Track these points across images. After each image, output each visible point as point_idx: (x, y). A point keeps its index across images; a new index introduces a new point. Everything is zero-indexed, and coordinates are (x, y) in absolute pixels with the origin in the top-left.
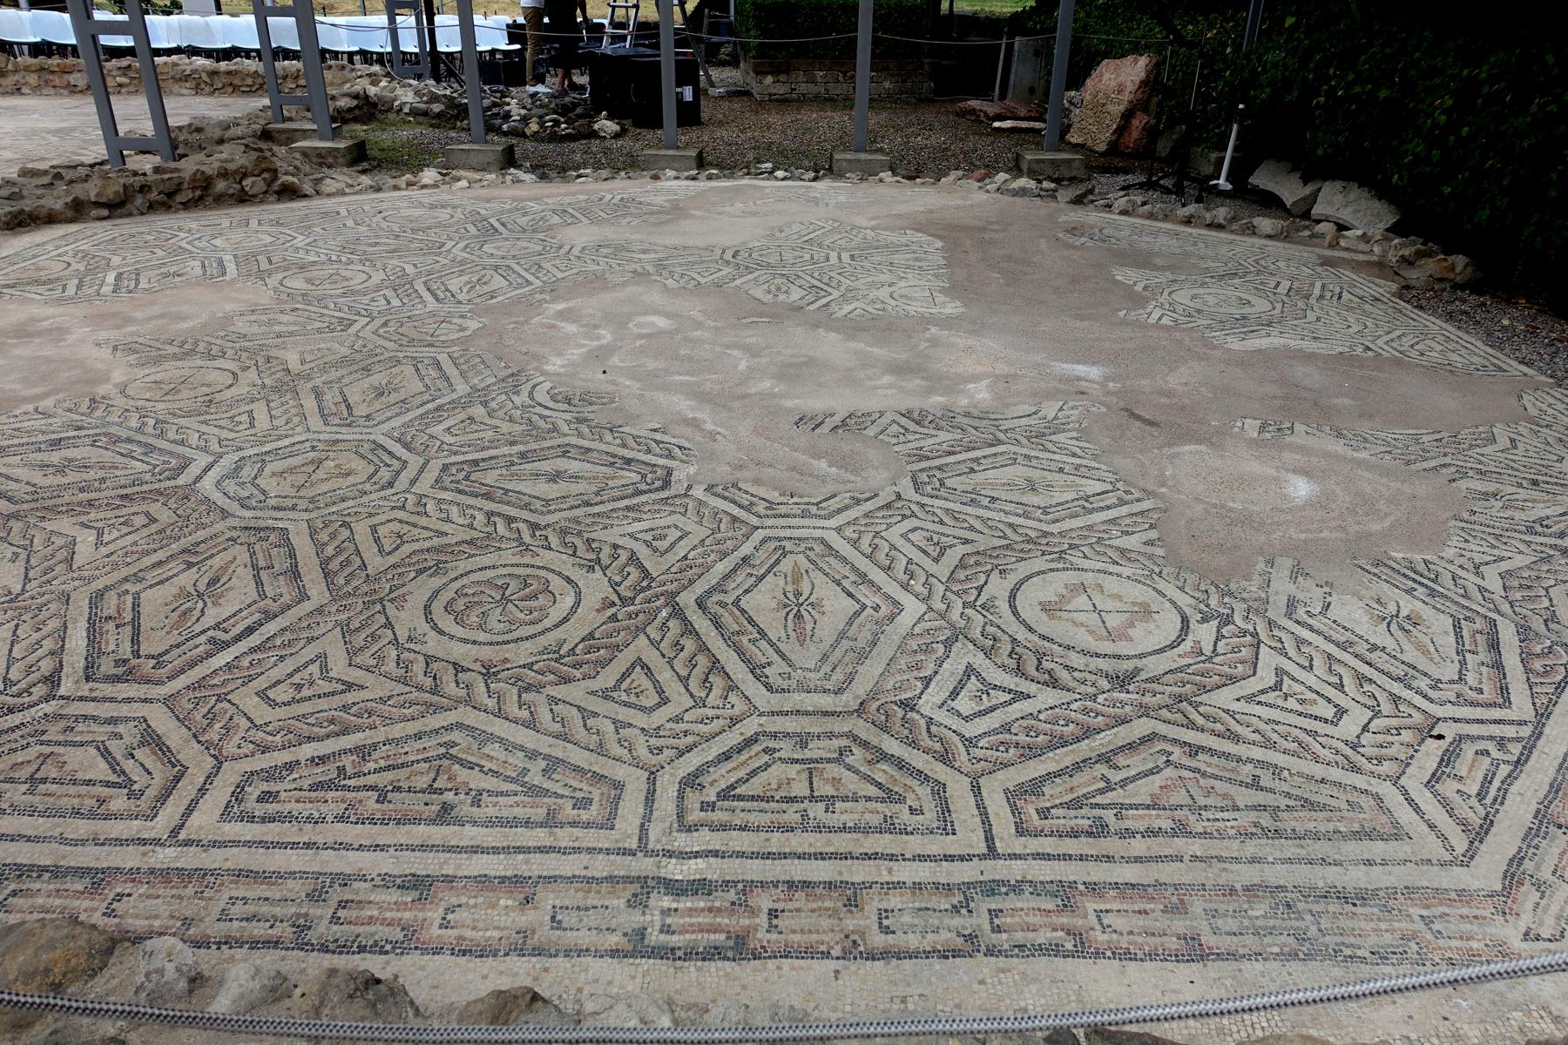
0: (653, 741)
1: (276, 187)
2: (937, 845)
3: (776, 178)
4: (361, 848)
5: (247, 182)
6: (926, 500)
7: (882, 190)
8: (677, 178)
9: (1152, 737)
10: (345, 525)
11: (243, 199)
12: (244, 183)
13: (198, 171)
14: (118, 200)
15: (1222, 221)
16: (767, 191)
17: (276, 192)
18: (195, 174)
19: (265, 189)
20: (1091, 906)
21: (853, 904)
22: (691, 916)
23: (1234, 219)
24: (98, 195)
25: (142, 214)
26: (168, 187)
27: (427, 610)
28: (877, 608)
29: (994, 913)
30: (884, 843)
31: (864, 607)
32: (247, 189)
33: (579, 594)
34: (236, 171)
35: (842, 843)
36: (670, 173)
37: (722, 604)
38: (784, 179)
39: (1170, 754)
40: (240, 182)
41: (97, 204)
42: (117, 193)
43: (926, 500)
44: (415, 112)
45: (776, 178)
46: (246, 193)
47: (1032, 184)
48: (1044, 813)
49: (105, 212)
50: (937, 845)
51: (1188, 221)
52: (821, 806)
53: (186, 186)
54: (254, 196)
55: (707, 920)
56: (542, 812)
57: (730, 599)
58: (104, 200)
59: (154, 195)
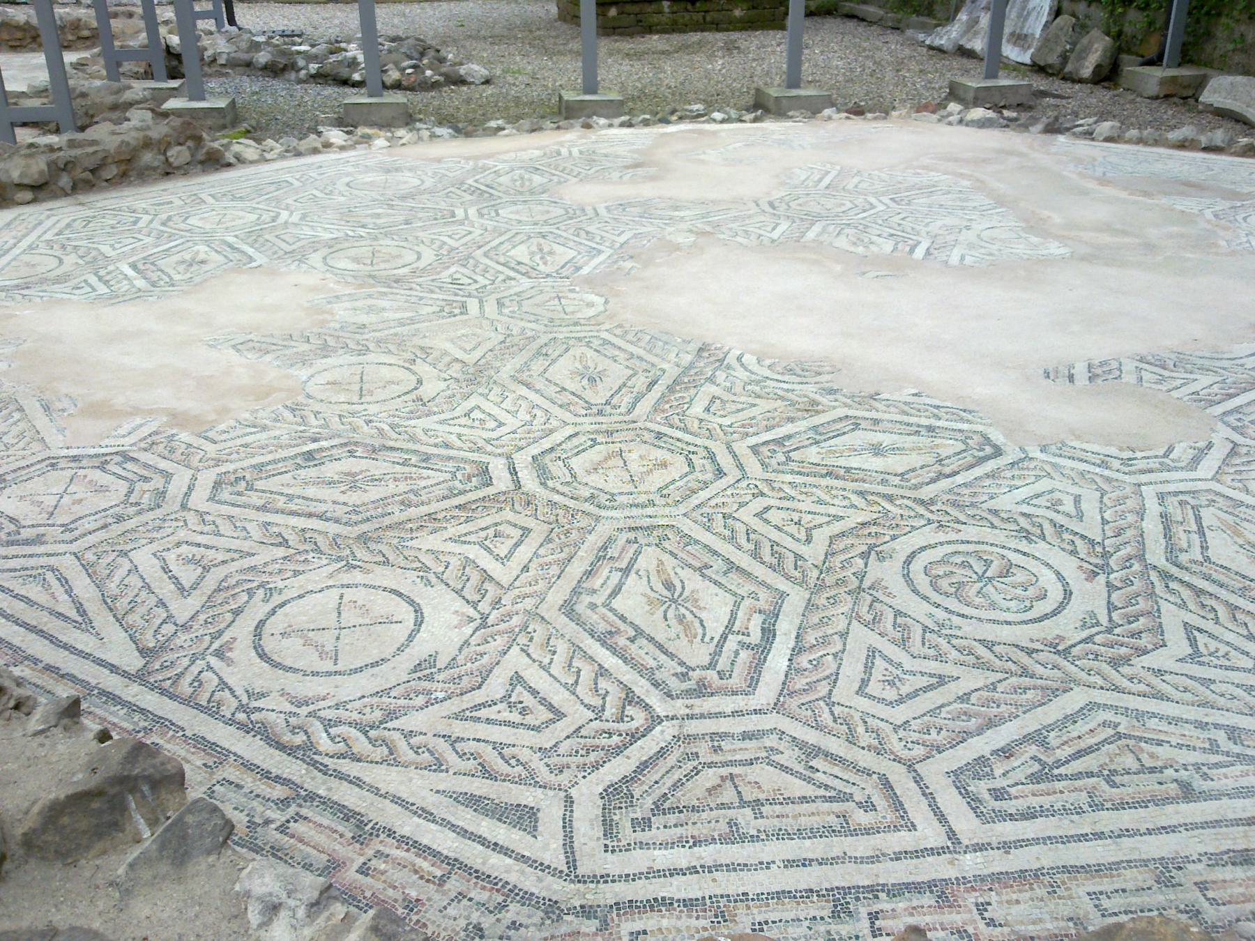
0: (554, 760)
1: (201, 155)
2: (902, 840)
3: (714, 120)
4: (1149, 832)
5: (172, 152)
6: (772, 476)
7: (831, 126)
8: (611, 126)
9: (1092, 706)
10: (124, 554)
11: (168, 172)
12: (169, 154)
13: (123, 142)
14: (43, 181)
15: (1219, 144)
16: (723, 134)
17: (202, 162)
18: (120, 146)
19: (189, 159)
20: (971, 899)
21: (841, 911)
22: (912, 915)
23: (1231, 142)
24: (21, 176)
25: (67, 195)
26: (91, 163)
27: (1068, 594)
28: (754, 596)
29: (874, 917)
30: (838, 845)
31: (604, 605)
32: (171, 160)
33: (418, 610)
34: (159, 142)
35: (1127, 818)
36: (602, 121)
37: (593, 606)
38: (723, 121)
39: (1116, 725)
40: (165, 153)
41: (21, 186)
42: (41, 173)
43: (772, 476)
44: (233, 64)
45: (714, 120)
46: (170, 165)
47: (990, 114)
48: (998, 794)
49: (28, 195)
50: (902, 840)
51: (1182, 145)
52: (748, 811)
53: (110, 160)
54: (178, 168)
55: (1122, 901)
56: (723, 827)
57: (599, 599)
58: (26, 181)
59: (79, 174)
